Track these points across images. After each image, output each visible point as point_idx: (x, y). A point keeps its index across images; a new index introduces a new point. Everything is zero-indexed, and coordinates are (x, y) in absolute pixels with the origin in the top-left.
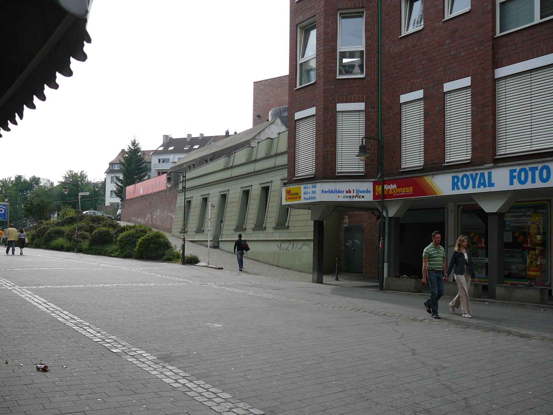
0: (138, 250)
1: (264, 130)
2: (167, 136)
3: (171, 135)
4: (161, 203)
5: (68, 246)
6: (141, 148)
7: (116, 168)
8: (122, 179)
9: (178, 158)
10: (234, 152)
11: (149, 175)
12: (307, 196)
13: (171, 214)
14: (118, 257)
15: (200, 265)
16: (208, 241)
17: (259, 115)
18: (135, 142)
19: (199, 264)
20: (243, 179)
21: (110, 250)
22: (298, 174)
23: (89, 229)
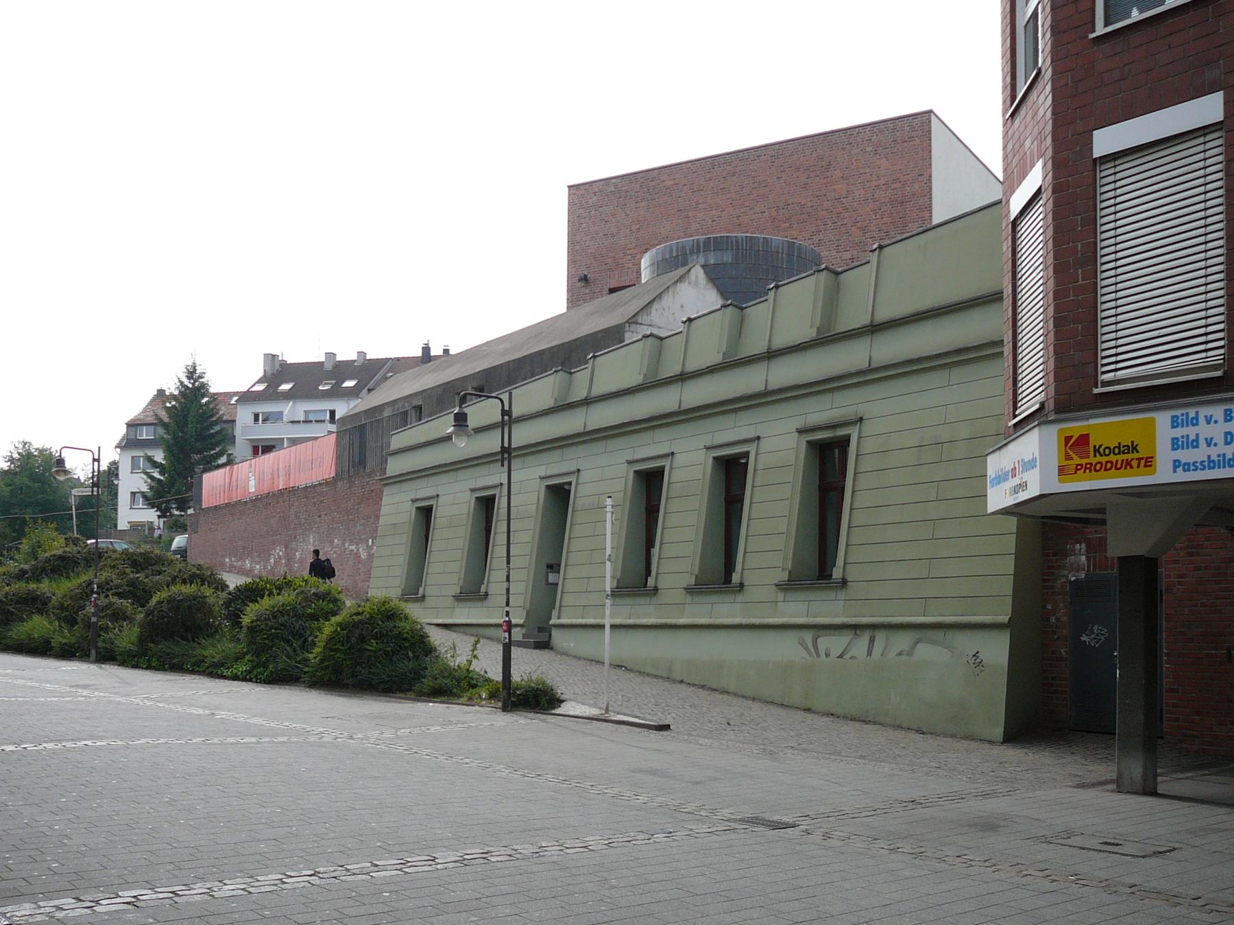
0: (322, 661)
1: (659, 296)
2: (274, 356)
3: (282, 354)
4: (320, 516)
5: (64, 641)
6: (210, 384)
7: (145, 435)
8: (164, 462)
9: (305, 411)
10: (591, 355)
11: (229, 452)
12: (1186, 455)
13: (353, 547)
14: (245, 679)
15: (558, 712)
16: (603, 627)
17: (585, 275)
18: (196, 370)
19: (564, 709)
20: (792, 404)
21: (214, 657)
22: (1117, 370)
23: (127, 589)
